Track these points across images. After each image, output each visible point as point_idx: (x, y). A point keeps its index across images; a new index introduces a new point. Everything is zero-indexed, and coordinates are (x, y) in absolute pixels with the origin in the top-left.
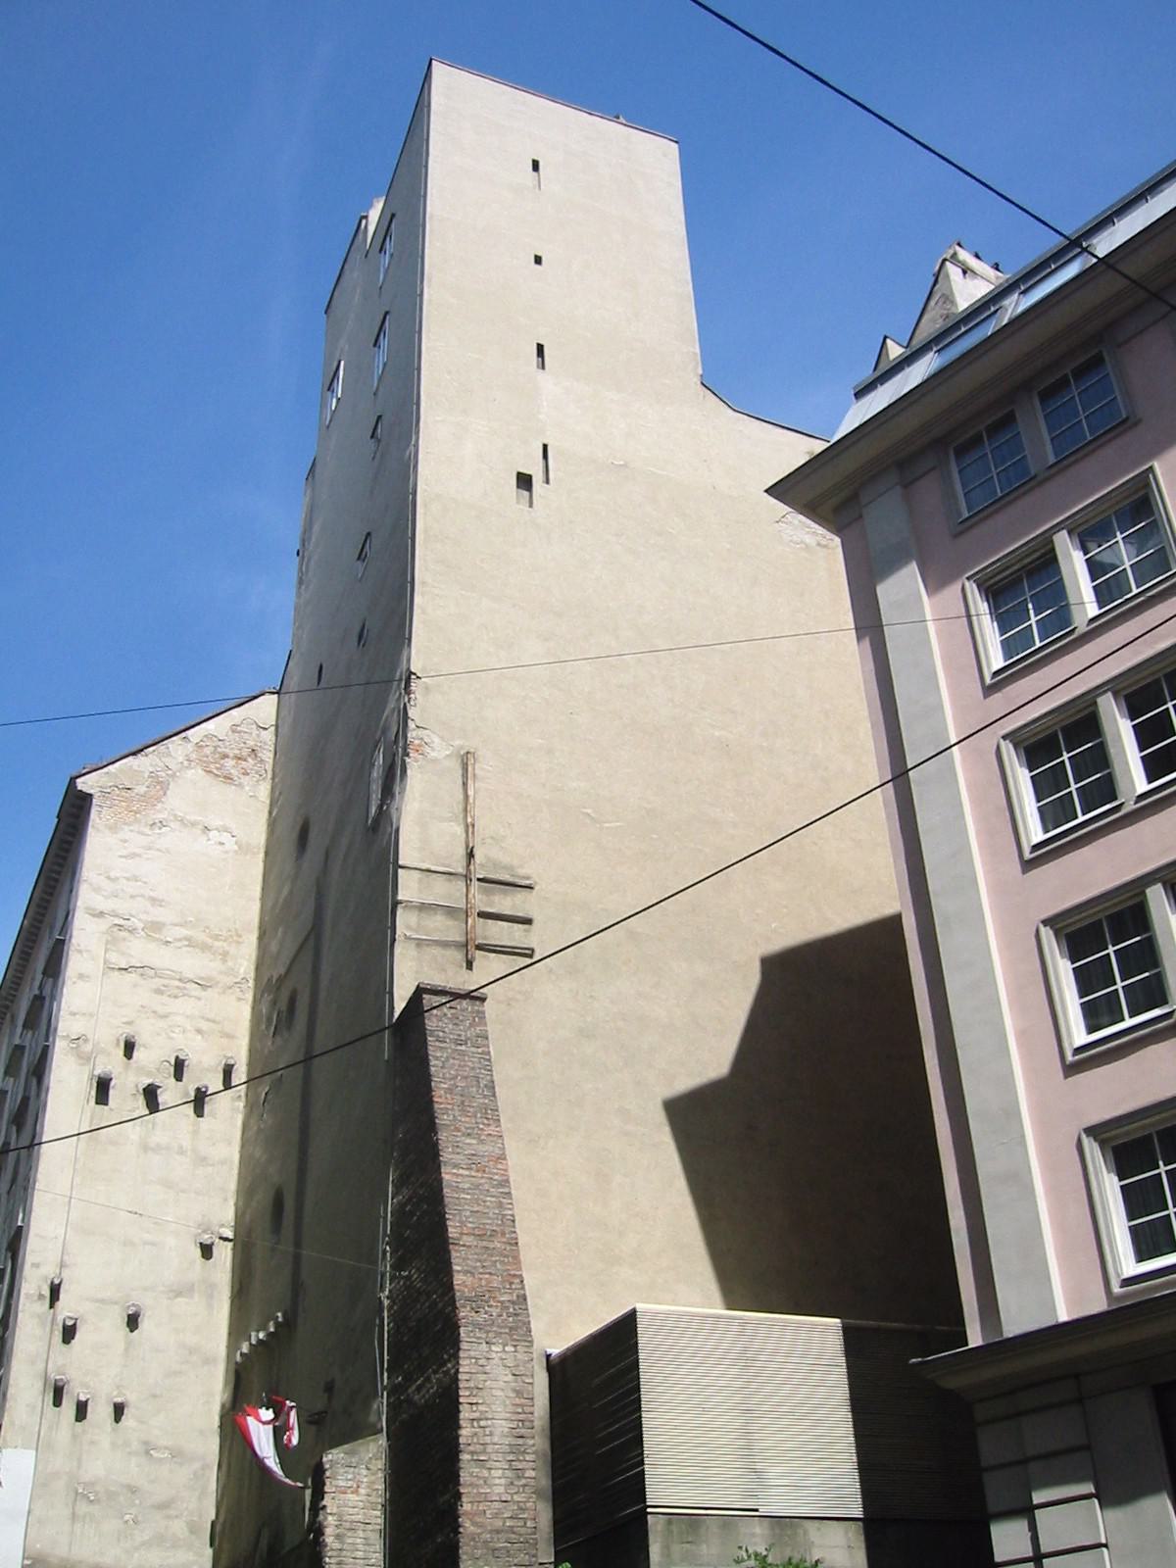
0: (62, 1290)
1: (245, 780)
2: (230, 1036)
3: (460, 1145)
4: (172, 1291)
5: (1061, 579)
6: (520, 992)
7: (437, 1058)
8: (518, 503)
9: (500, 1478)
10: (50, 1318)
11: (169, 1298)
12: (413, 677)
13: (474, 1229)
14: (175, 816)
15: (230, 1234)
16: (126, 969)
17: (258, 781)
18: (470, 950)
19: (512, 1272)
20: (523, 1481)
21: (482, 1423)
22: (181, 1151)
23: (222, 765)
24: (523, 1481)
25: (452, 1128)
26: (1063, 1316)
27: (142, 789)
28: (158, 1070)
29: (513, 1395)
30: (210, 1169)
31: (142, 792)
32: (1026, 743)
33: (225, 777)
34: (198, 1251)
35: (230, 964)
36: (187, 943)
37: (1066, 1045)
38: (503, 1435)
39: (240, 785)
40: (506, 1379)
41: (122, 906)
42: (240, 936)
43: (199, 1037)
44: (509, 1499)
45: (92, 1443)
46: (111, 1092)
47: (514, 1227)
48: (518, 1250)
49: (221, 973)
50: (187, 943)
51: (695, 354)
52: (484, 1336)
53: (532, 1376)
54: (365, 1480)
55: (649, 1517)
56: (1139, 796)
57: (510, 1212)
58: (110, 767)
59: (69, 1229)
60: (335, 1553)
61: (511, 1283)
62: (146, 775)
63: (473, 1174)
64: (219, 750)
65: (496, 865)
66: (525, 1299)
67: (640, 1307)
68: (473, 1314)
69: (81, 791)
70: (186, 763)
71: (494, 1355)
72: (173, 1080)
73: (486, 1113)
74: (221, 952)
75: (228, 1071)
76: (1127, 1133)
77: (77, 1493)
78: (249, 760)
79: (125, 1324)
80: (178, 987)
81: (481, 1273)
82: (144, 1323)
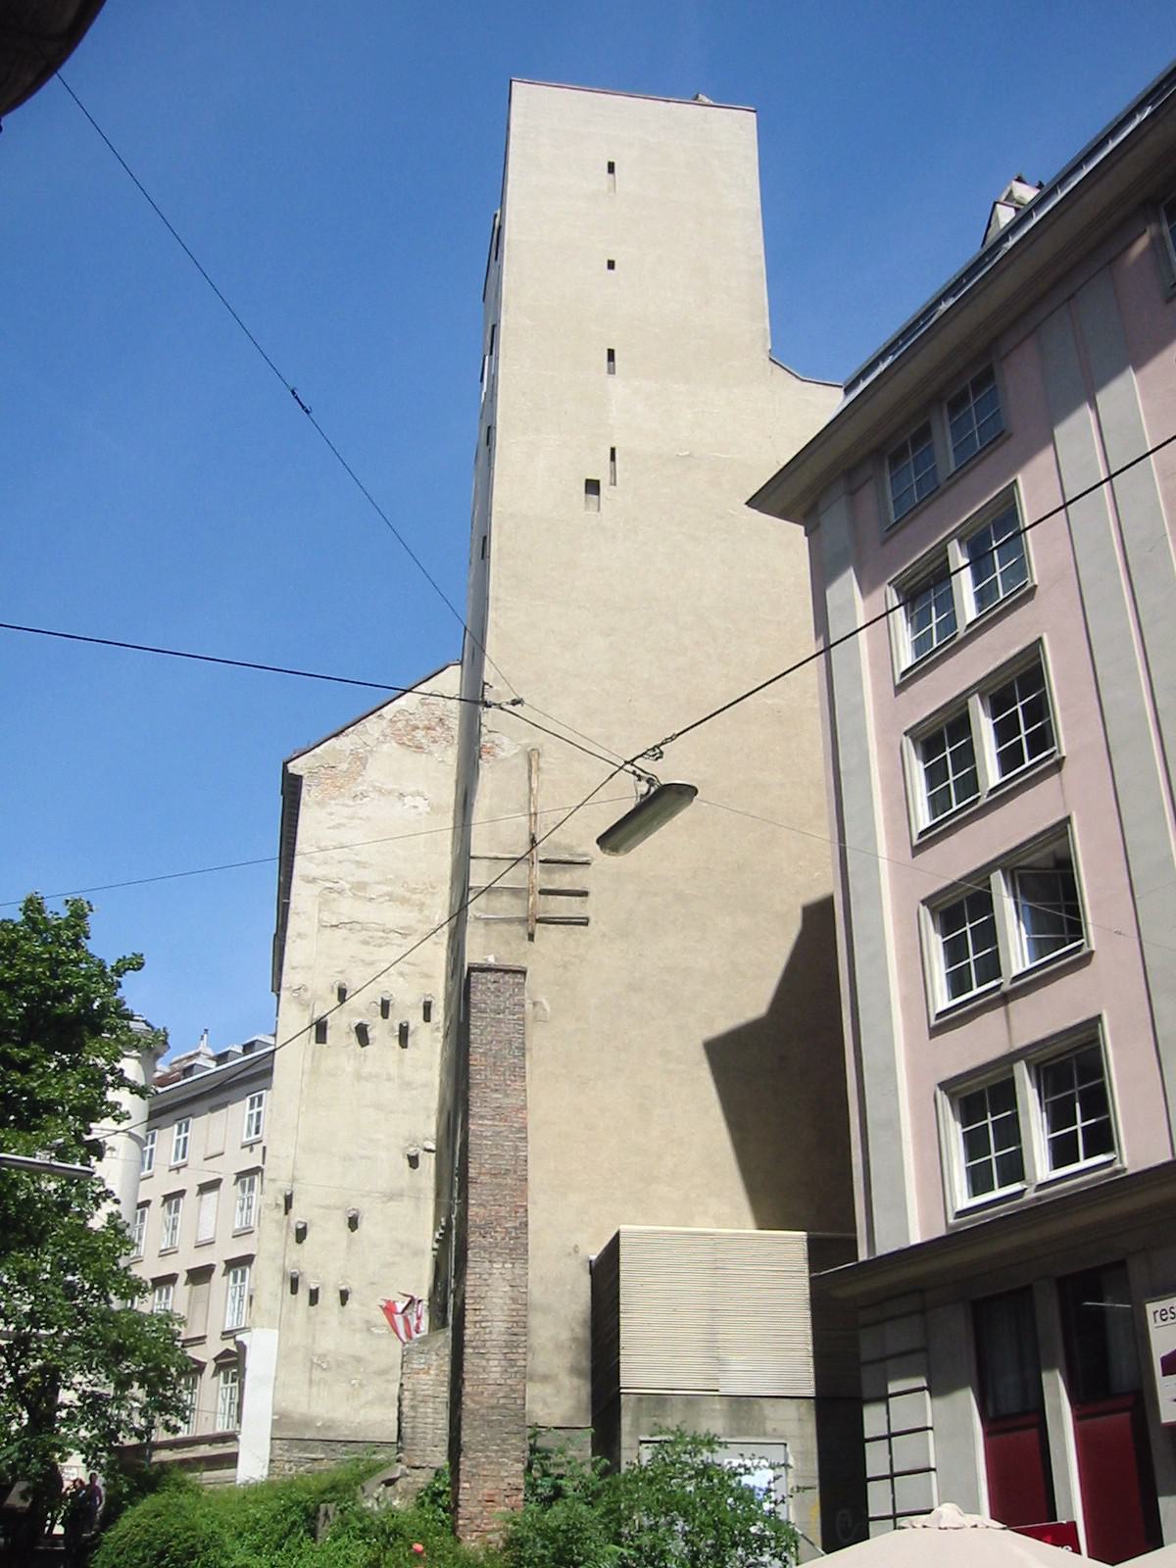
0: (294, 1200)
1: (434, 747)
2: (427, 976)
3: (488, 1099)
4: (384, 1196)
5: (951, 588)
6: (575, 956)
7: (477, 1027)
8: (586, 509)
9: (496, 1366)
10: (285, 1223)
11: (383, 1202)
12: (487, 687)
13: (491, 1169)
14: (374, 787)
15: (432, 1146)
16: (336, 926)
17: (446, 747)
18: (533, 924)
19: (518, 1204)
20: (516, 1369)
21: (483, 1325)
22: (389, 1079)
23: (414, 736)
24: (516, 1369)
25: (483, 1085)
26: (916, 1238)
27: (344, 766)
28: (367, 1010)
29: (509, 1302)
30: (414, 1092)
31: (345, 769)
32: (921, 739)
33: (417, 747)
34: (406, 1162)
35: (426, 912)
36: (387, 898)
37: (931, 1011)
38: (500, 1334)
39: (430, 753)
40: (505, 1290)
41: (332, 871)
42: (434, 888)
43: (401, 979)
44: (503, 1382)
45: (324, 1323)
46: (328, 1032)
47: (526, 1165)
48: (526, 1185)
49: (419, 921)
50: (387, 898)
51: (765, 330)
52: (487, 1256)
53: (526, 1287)
54: (435, 1363)
55: (622, 1396)
56: (991, 790)
57: (524, 1154)
58: (317, 750)
59: (298, 1150)
60: (410, 1420)
61: (516, 1212)
62: (348, 753)
63: (496, 1123)
64: (411, 723)
65: (557, 846)
66: (526, 1225)
67: (623, 1228)
68: (481, 1239)
69: (292, 774)
70: (381, 738)
71: (495, 1271)
72: (380, 1018)
73: (515, 1071)
74: (417, 902)
75: (427, 1008)
76: (970, 1087)
77: (312, 1362)
78: (437, 728)
79: (347, 1226)
80: (382, 938)
81: (492, 1205)
82: (363, 1225)
